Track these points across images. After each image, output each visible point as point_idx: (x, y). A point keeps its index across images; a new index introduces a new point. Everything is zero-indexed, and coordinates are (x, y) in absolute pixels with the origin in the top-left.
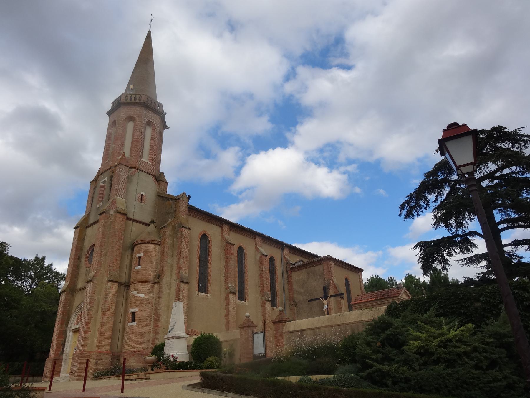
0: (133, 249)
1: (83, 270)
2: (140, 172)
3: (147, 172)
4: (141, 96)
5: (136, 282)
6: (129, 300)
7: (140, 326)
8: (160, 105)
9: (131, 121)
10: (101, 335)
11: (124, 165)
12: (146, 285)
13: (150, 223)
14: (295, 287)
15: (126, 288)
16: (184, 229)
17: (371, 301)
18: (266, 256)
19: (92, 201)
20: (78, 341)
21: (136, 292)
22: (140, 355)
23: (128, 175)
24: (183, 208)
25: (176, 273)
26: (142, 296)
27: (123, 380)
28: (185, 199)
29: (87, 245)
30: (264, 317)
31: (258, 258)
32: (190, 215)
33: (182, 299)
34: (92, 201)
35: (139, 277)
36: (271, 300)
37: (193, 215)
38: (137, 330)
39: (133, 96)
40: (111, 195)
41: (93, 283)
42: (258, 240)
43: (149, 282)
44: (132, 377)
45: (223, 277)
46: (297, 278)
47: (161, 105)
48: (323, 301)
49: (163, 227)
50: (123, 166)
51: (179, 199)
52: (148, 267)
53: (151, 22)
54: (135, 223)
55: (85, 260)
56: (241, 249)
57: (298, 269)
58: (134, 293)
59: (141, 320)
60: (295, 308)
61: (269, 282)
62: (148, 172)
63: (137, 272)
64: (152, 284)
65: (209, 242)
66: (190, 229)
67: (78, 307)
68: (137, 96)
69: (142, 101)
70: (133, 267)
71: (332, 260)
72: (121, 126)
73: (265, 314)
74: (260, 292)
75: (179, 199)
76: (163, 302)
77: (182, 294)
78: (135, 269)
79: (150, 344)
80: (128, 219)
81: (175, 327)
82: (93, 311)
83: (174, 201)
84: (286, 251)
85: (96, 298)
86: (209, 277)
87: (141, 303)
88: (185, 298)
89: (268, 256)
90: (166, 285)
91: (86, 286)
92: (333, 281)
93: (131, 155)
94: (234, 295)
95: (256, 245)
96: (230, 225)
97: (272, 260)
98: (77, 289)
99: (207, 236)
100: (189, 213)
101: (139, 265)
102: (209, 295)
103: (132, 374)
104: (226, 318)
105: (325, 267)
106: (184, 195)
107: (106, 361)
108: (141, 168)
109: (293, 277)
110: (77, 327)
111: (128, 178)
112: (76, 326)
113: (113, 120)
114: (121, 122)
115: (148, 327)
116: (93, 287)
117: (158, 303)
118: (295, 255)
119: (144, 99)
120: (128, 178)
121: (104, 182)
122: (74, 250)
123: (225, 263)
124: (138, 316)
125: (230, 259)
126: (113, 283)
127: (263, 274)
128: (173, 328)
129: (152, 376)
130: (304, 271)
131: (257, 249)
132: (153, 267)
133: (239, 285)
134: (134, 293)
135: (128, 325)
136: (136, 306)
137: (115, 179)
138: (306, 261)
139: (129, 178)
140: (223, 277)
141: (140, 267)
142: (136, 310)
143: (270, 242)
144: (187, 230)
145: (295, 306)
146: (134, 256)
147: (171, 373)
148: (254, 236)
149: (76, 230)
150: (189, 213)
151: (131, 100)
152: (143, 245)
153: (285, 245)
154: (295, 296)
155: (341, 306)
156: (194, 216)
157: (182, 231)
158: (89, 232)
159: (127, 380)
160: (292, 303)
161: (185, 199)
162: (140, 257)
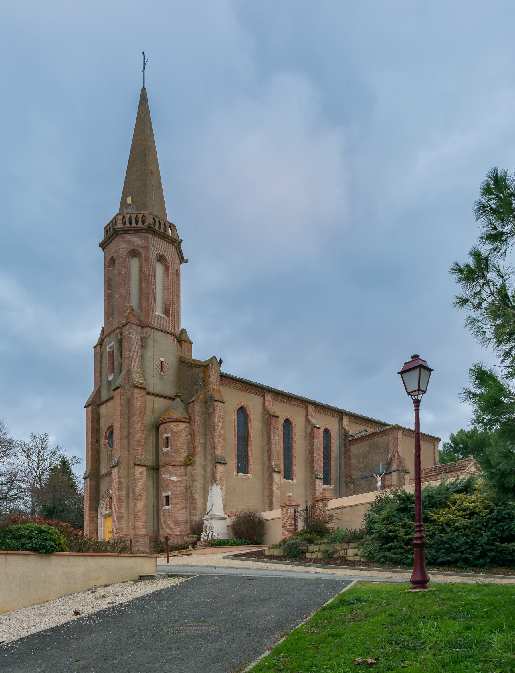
0: (157, 428)
1: (103, 454)
2: (156, 331)
3: (165, 330)
4: (144, 215)
5: (166, 465)
6: (161, 484)
7: (176, 509)
8: (172, 227)
9: (135, 256)
10: (136, 519)
11: (134, 324)
12: (178, 468)
13: (175, 397)
14: (354, 462)
15: (155, 472)
16: (217, 403)
17: (433, 475)
18: (318, 429)
19: (101, 372)
20: (112, 526)
21: (167, 475)
22: (179, 537)
23: (141, 337)
24: (214, 377)
25: (211, 453)
26: (175, 479)
27: (168, 557)
28: (215, 364)
29: (104, 426)
30: (313, 496)
31: (309, 430)
32: (223, 384)
33: (219, 481)
34: (101, 372)
35: (168, 459)
36: (322, 477)
37: (226, 384)
38: (173, 513)
39: (134, 216)
40: (123, 365)
41: (119, 468)
42: (310, 408)
43: (180, 464)
44: (173, 555)
45: (265, 454)
46: (356, 452)
47: (174, 226)
48: (377, 477)
49: (191, 402)
50: (133, 325)
51: (208, 365)
52: (178, 448)
53: (144, 68)
54: (157, 398)
55: (105, 444)
56: (288, 423)
57: (359, 441)
58: (166, 476)
59: (176, 504)
60: (352, 485)
61: (321, 458)
62: (167, 331)
63: (166, 453)
64: (184, 467)
65: (248, 416)
66: (224, 403)
67: (105, 492)
68: (139, 215)
69: (146, 224)
70: (160, 450)
71: (400, 430)
72: (122, 266)
73: (315, 493)
74: (310, 469)
75: (208, 365)
76: (198, 484)
77: (218, 476)
78: (164, 451)
79: (188, 526)
80: (148, 393)
81: (212, 509)
82: (123, 496)
83: (203, 368)
84: (346, 420)
85: (124, 483)
86: (250, 455)
87: (174, 486)
88: (222, 480)
89: (320, 428)
90: (200, 467)
91: (111, 470)
92: (398, 454)
93: (140, 308)
94: (279, 474)
95: (307, 415)
96: (273, 393)
97: (327, 432)
98: (102, 475)
99: (246, 408)
100: (222, 383)
101: (167, 447)
102: (249, 475)
103: (173, 552)
104: (269, 499)
105: (391, 438)
106: (214, 360)
107: (143, 542)
108: (156, 325)
109: (351, 451)
110: (107, 512)
111: (142, 342)
112: (106, 511)
113: (110, 257)
114: (121, 260)
115: (184, 510)
116: (119, 472)
117: (192, 486)
118: (357, 425)
119: (149, 220)
120: (141, 341)
121: (112, 347)
122: (90, 432)
123: (268, 439)
124: (172, 500)
125: (274, 434)
126: (140, 467)
127: (313, 449)
128: (211, 510)
129: (193, 552)
130: (365, 443)
131: (308, 420)
132: (184, 448)
133: (285, 463)
134: (166, 476)
135: (163, 509)
136: (169, 490)
137: (125, 344)
138: (370, 430)
139: (143, 343)
140: (265, 454)
141: (169, 449)
142: (169, 493)
143: (325, 411)
144: (221, 404)
145: (352, 483)
146: (160, 437)
147: (211, 549)
148: (305, 405)
149: (87, 409)
150: (222, 383)
151: (131, 223)
152: (169, 424)
153: (344, 414)
154: (353, 472)
155: (404, 481)
156: (228, 385)
157: (214, 405)
158: (103, 410)
159: (170, 556)
160: (349, 479)
161: (215, 364)
162: (167, 438)
